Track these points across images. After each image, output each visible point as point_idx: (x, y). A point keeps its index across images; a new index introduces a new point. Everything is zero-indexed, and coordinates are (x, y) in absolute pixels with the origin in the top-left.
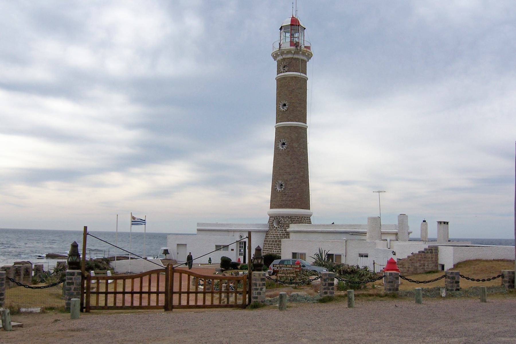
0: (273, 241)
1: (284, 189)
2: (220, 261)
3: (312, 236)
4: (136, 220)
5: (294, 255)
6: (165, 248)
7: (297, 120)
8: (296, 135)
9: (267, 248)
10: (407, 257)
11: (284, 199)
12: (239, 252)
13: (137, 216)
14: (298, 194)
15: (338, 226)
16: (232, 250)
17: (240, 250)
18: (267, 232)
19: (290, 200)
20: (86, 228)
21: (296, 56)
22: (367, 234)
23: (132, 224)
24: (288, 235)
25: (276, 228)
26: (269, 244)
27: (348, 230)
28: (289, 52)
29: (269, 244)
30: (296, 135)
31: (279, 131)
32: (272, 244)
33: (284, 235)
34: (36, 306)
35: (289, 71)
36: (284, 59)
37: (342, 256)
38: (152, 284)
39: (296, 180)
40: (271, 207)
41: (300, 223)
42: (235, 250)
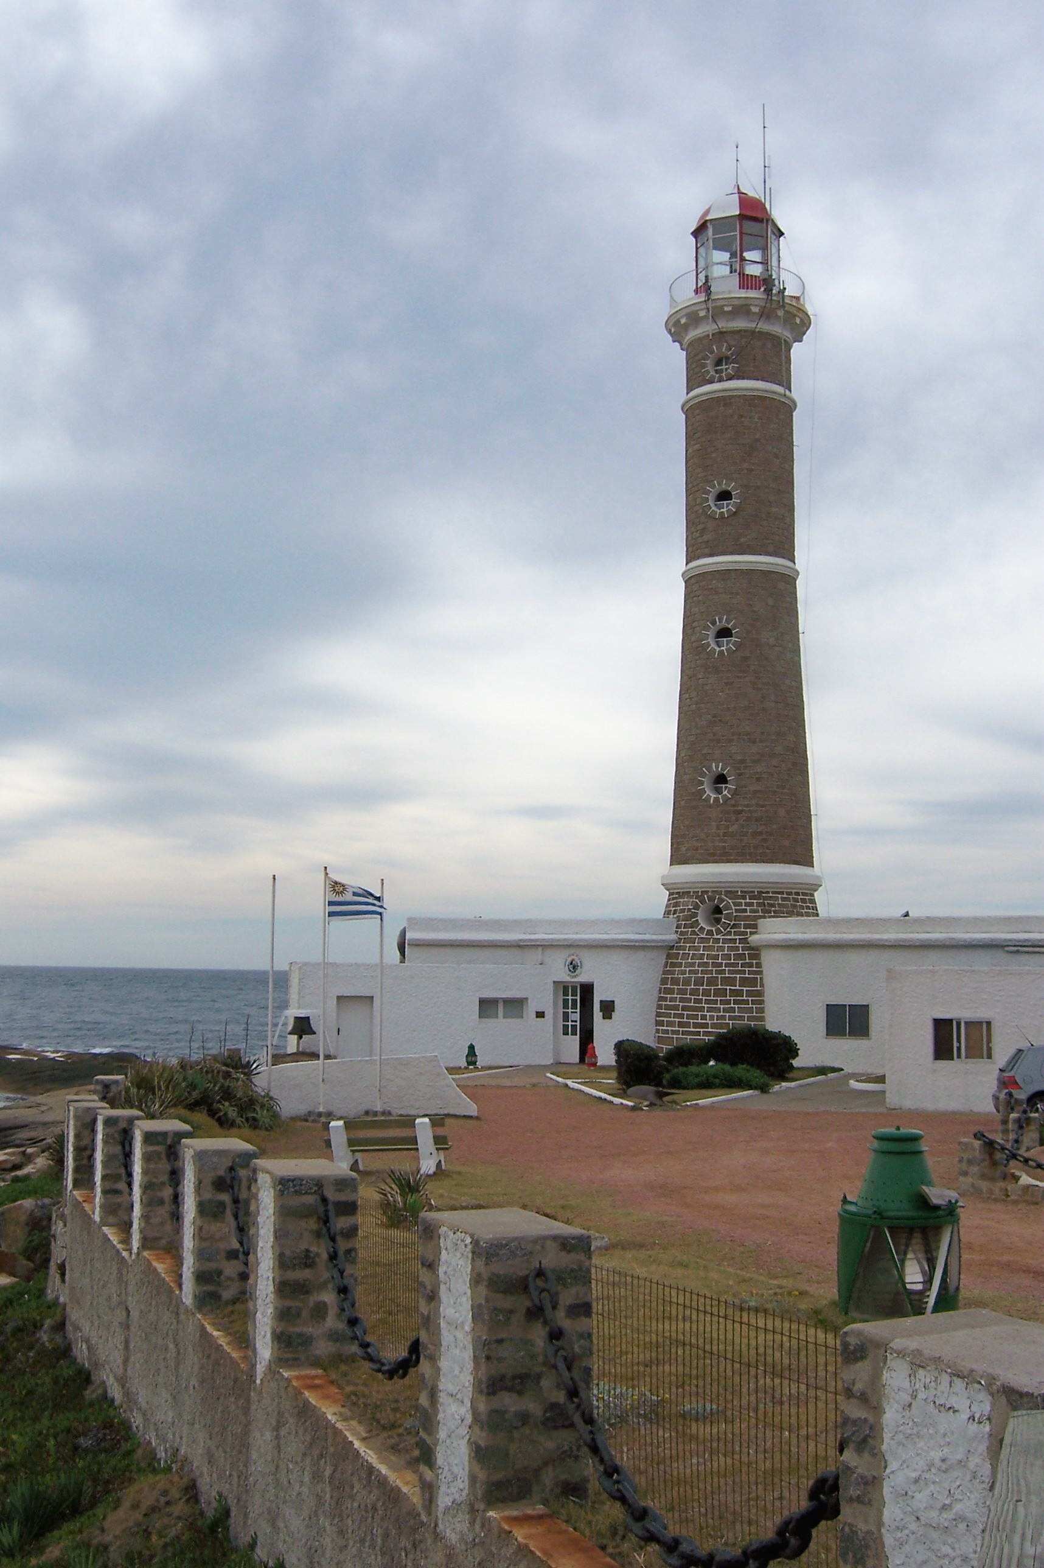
0: (699, 982)
1: (735, 793)
3: (854, 958)
4: (348, 897)
7: (771, 549)
8: (770, 601)
9: (676, 1008)
10: (174, 1061)
11: (733, 828)
12: (561, 1023)
13: (353, 881)
14: (782, 812)
15: (918, 921)
16: (540, 1015)
17: (566, 1017)
18: (670, 951)
19: (755, 834)
21: (764, 326)
23: (331, 914)
24: (757, 956)
25: (710, 933)
26: (680, 991)
27: (1003, 936)
28: (741, 309)
29: (680, 991)
30: (770, 601)
31: (697, 587)
32: (694, 992)
33: (741, 957)
35: (739, 375)
36: (721, 334)
38: (886, 1143)
39: (774, 762)
40: (678, 857)
41: (791, 914)
42: (549, 1015)
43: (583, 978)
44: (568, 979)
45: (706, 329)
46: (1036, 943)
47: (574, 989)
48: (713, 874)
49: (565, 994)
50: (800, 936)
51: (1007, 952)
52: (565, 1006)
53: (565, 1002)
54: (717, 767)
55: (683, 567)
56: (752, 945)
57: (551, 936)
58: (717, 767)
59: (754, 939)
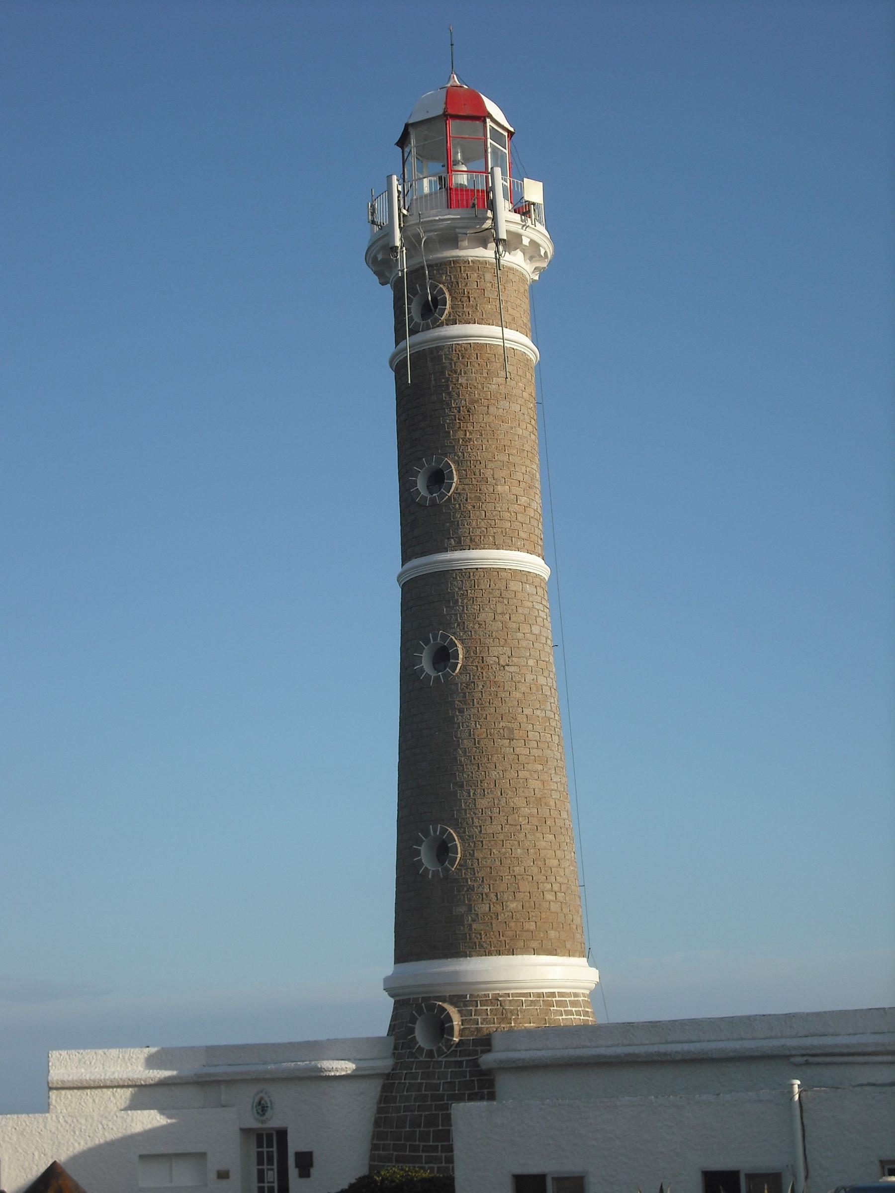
16: (223, 1175)
17: (261, 1179)
43: (275, 1122)
44: (259, 1125)
46: (836, 1050)
47: (269, 1136)
49: (260, 1144)
51: (795, 1065)
52: (260, 1162)
53: (260, 1155)
54: (435, 830)
55: (390, 347)
56: (484, 1067)
58: (435, 830)
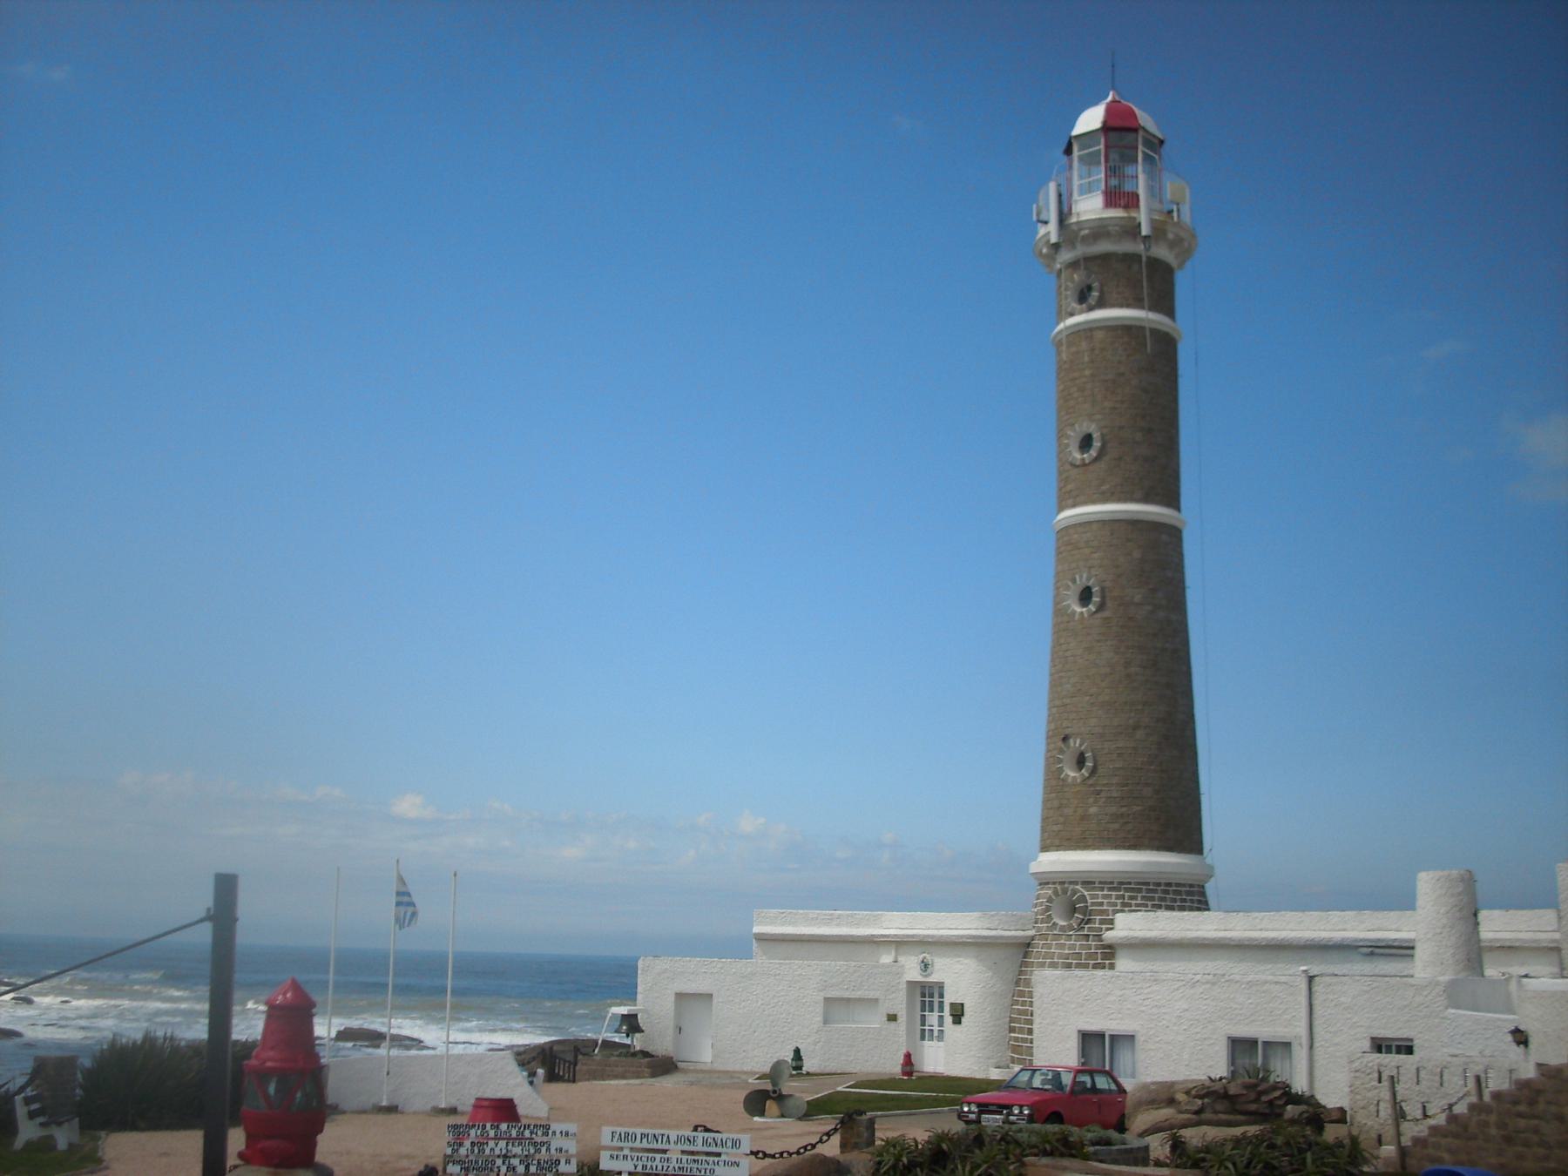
1: (1093, 771)
2: (472, 1101)
5: (1089, 1040)
6: (624, 1010)
16: (892, 1018)
20: (226, 887)
22: (1418, 952)
25: (1062, 928)
34: (277, 1091)
37: (1295, 1047)
42: (902, 1019)
44: (920, 979)
45: (1066, 256)
48: (1100, 863)
49: (923, 995)
50: (1338, 936)
57: (993, 933)
59: (1109, 936)
